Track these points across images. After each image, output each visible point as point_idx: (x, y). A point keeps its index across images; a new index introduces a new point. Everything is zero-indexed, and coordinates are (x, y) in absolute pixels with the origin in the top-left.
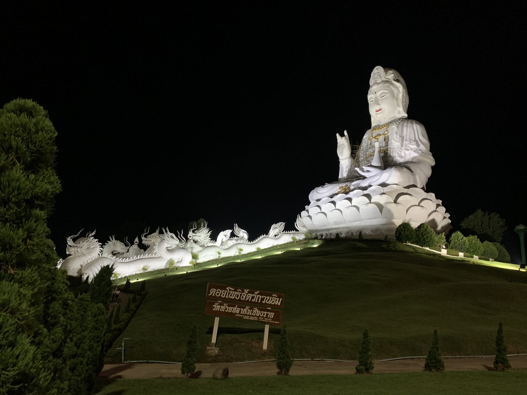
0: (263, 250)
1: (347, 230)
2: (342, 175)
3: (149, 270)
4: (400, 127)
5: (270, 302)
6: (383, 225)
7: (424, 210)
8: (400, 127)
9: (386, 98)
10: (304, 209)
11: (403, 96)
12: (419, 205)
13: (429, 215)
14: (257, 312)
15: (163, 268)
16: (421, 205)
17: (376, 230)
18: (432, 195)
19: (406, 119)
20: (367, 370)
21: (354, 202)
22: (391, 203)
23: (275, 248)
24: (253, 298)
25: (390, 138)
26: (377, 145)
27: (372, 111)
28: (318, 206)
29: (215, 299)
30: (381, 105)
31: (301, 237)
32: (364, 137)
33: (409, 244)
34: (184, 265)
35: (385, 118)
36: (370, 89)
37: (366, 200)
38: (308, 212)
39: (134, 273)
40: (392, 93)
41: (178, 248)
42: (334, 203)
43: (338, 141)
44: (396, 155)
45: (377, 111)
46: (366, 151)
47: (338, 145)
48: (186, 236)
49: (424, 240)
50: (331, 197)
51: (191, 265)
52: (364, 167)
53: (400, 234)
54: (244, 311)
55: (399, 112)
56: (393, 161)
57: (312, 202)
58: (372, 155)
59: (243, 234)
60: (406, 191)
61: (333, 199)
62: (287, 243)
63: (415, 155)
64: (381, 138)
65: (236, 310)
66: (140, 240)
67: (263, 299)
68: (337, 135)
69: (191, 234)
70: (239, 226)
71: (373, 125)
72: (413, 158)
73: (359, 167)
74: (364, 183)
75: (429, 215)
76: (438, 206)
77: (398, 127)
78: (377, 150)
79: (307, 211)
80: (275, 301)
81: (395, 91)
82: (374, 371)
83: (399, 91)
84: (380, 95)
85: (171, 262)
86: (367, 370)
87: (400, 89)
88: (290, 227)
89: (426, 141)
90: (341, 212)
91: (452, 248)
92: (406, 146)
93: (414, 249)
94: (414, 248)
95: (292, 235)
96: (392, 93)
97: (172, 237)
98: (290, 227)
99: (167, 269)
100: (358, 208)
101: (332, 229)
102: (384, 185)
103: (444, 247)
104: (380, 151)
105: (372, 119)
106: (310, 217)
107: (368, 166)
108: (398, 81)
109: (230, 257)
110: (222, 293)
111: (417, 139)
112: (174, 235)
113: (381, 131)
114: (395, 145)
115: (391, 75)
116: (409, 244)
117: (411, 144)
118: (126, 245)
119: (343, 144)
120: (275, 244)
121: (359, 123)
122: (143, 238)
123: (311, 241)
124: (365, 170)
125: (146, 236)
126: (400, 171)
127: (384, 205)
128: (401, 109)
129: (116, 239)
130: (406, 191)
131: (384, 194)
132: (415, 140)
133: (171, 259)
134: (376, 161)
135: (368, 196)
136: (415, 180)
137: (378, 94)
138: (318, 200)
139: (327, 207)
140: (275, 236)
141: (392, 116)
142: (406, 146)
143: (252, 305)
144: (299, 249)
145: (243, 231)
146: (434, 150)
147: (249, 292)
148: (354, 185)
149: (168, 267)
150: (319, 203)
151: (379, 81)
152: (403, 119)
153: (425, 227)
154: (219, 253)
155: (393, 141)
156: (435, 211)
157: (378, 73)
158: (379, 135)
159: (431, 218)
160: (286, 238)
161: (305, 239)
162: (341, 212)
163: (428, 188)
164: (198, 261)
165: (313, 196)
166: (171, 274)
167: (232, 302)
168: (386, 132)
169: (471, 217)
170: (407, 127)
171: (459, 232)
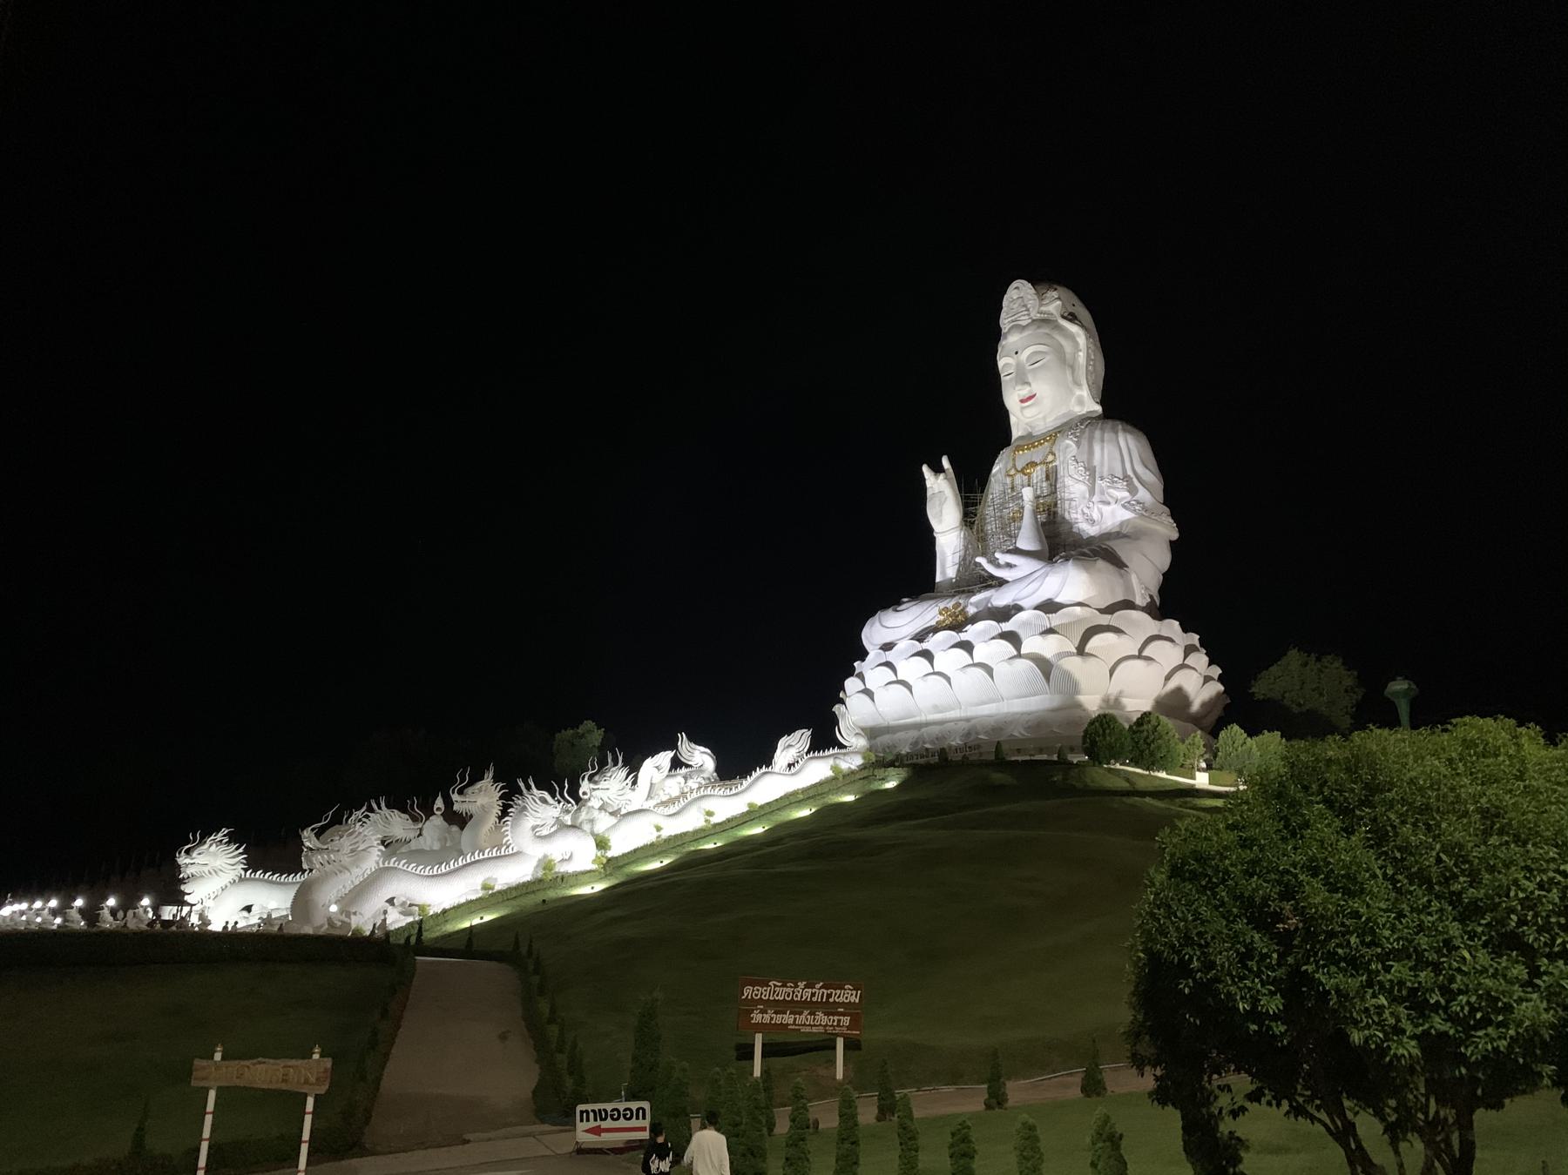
0: (762, 807)
1: (966, 725)
2: (943, 572)
3: (497, 888)
4: (1085, 442)
5: (841, 1000)
6: (1053, 710)
7: (1149, 669)
8: (1085, 442)
9: (1045, 366)
10: (850, 672)
11: (1088, 355)
12: (1139, 657)
13: (1168, 678)
14: (821, 1018)
15: (529, 878)
16: (1145, 653)
17: (1038, 725)
18: (1172, 627)
19: (1099, 418)
20: (1000, 1104)
21: (980, 653)
22: (1069, 654)
23: (793, 799)
24: (813, 995)
25: (1061, 473)
26: (1028, 494)
27: (1012, 398)
28: (888, 664)
29: (754, 1002)
30: (1034, 385)
31: (852, 763)
32: (994, 470)
33: (1118, 766)
34: (579, 869)
35: (1044, 418)
36: (1003, 342)
37: (1007, 648)
38: (863, 680)
39: (463, 900)
40: (1059, 352)
41: (562, 827)
42: (927, 655)
43: (928, 484)
44: (1079, 516)
45: (1022, 401)
46: (1003, 506)
47: (929, 493)
48: (574, 793)
49: (1152, 754)
50: (920, 637)
51: (594, 867)
52: (997, 555)
53: (1093, 743)
54: (801, 1019)
55: (1080, 402)
56: (1070, 532)
57: (874, 654)
58: (1017, 518)
59: (701, 758)
60: (1105, 620)
61: (925, 646)
62: (820, 784)
63: (1127, 515)
64: (1038, 474)
65: (787, 1019)
66: (449, 803)
67: (829, 996)
68: (925, 468)
69: (585, 786)
70: (691, 739)
71: (1016, 433)
72: (1122, 524)
73: (983, 554)
74: (1000, 598)
75: (1168, 678)
76: (1189, 650)
77: (1078, 444)
78: (1028, 507)
79: (861, 677)
80: (850, 996)
81: (1067, 346)
82: (1010, 1103)
83: (1076, 343)
84: (1029, 358)
85: (547, 864)
86: (1000, 1104)
87: (1080, 341)
88: (825, 739)
89: (1152, 477)
90: (948, 679)
91: (1221, 769)
92: (1102, 493)
93: (1128, 780)
94: (1128, 777)
95: (831, 761)
96: (1059, 352)
97: (544, 801)
98: (825, 739)
99: (540, 881)
100: (988, 670)
101: (927, 724)
102: (1049, 607)
103: (1204, 765)
104: (1035, 512)
105: (1013, 420)
106: (868, 693)
107: (1009, 552)
108: (1072, 318)
109: (685, 834)
110: (763, 993)
111: (1130, 472)
112: (546, 795)
113: (1036, 455)
114: (1074, 488)
115: (1055, 303)
116: (1118, 766)
117: (1112, 487)
118: (415, 819)
119: (940, 490)
120: (791, 790)
121: (976, 433)
122: (455, 797)
123: (880, 773)
124: (1002, 562)
125: (461, 792)
126: (1087, 569)
127: (1053, 660)
128: (1084, 392)
129: (388, 807)
130: (1105, 620)
131: (1051, 631)
132: (1126, 478)
133: (545, 856)
134: (1026, 541)
135: (1012, 638)
136: (1128, 587)
137: (1024, 356)
138: (887, 647)
139: (912, 669)
140: (790, 766)
141: (1063, 410)
142: (1102, 493)
143: (812, 1007)
144: (850, 798)
145: (702, 749)
146: (1175, 498)
147: (806, 986)
148: (976, 605)
149: (540, 874)
150: (890, 656)
151: (1025, 321)
152: (1088, 420)
153: (1154, 722)
154: (659, 829)
155: (1068, 481)
156: (1182, 666)
157: (1019, 299)
158: (1033, 464)
159: (1172, 685)
160: (818, 770)
161: (863, 768)
162: (948, 679)
163: (1161, 609)
164: (610, 854)
165: (874, 633)
166: (551, 894)
167: (780, 1006)
168: (1050, 458)
169: (1273, 669)
170: (1102, 441)
171: (1236, 727)
